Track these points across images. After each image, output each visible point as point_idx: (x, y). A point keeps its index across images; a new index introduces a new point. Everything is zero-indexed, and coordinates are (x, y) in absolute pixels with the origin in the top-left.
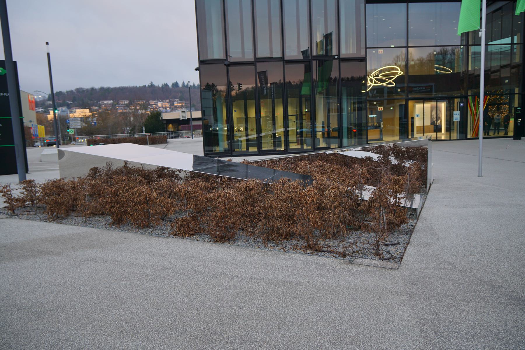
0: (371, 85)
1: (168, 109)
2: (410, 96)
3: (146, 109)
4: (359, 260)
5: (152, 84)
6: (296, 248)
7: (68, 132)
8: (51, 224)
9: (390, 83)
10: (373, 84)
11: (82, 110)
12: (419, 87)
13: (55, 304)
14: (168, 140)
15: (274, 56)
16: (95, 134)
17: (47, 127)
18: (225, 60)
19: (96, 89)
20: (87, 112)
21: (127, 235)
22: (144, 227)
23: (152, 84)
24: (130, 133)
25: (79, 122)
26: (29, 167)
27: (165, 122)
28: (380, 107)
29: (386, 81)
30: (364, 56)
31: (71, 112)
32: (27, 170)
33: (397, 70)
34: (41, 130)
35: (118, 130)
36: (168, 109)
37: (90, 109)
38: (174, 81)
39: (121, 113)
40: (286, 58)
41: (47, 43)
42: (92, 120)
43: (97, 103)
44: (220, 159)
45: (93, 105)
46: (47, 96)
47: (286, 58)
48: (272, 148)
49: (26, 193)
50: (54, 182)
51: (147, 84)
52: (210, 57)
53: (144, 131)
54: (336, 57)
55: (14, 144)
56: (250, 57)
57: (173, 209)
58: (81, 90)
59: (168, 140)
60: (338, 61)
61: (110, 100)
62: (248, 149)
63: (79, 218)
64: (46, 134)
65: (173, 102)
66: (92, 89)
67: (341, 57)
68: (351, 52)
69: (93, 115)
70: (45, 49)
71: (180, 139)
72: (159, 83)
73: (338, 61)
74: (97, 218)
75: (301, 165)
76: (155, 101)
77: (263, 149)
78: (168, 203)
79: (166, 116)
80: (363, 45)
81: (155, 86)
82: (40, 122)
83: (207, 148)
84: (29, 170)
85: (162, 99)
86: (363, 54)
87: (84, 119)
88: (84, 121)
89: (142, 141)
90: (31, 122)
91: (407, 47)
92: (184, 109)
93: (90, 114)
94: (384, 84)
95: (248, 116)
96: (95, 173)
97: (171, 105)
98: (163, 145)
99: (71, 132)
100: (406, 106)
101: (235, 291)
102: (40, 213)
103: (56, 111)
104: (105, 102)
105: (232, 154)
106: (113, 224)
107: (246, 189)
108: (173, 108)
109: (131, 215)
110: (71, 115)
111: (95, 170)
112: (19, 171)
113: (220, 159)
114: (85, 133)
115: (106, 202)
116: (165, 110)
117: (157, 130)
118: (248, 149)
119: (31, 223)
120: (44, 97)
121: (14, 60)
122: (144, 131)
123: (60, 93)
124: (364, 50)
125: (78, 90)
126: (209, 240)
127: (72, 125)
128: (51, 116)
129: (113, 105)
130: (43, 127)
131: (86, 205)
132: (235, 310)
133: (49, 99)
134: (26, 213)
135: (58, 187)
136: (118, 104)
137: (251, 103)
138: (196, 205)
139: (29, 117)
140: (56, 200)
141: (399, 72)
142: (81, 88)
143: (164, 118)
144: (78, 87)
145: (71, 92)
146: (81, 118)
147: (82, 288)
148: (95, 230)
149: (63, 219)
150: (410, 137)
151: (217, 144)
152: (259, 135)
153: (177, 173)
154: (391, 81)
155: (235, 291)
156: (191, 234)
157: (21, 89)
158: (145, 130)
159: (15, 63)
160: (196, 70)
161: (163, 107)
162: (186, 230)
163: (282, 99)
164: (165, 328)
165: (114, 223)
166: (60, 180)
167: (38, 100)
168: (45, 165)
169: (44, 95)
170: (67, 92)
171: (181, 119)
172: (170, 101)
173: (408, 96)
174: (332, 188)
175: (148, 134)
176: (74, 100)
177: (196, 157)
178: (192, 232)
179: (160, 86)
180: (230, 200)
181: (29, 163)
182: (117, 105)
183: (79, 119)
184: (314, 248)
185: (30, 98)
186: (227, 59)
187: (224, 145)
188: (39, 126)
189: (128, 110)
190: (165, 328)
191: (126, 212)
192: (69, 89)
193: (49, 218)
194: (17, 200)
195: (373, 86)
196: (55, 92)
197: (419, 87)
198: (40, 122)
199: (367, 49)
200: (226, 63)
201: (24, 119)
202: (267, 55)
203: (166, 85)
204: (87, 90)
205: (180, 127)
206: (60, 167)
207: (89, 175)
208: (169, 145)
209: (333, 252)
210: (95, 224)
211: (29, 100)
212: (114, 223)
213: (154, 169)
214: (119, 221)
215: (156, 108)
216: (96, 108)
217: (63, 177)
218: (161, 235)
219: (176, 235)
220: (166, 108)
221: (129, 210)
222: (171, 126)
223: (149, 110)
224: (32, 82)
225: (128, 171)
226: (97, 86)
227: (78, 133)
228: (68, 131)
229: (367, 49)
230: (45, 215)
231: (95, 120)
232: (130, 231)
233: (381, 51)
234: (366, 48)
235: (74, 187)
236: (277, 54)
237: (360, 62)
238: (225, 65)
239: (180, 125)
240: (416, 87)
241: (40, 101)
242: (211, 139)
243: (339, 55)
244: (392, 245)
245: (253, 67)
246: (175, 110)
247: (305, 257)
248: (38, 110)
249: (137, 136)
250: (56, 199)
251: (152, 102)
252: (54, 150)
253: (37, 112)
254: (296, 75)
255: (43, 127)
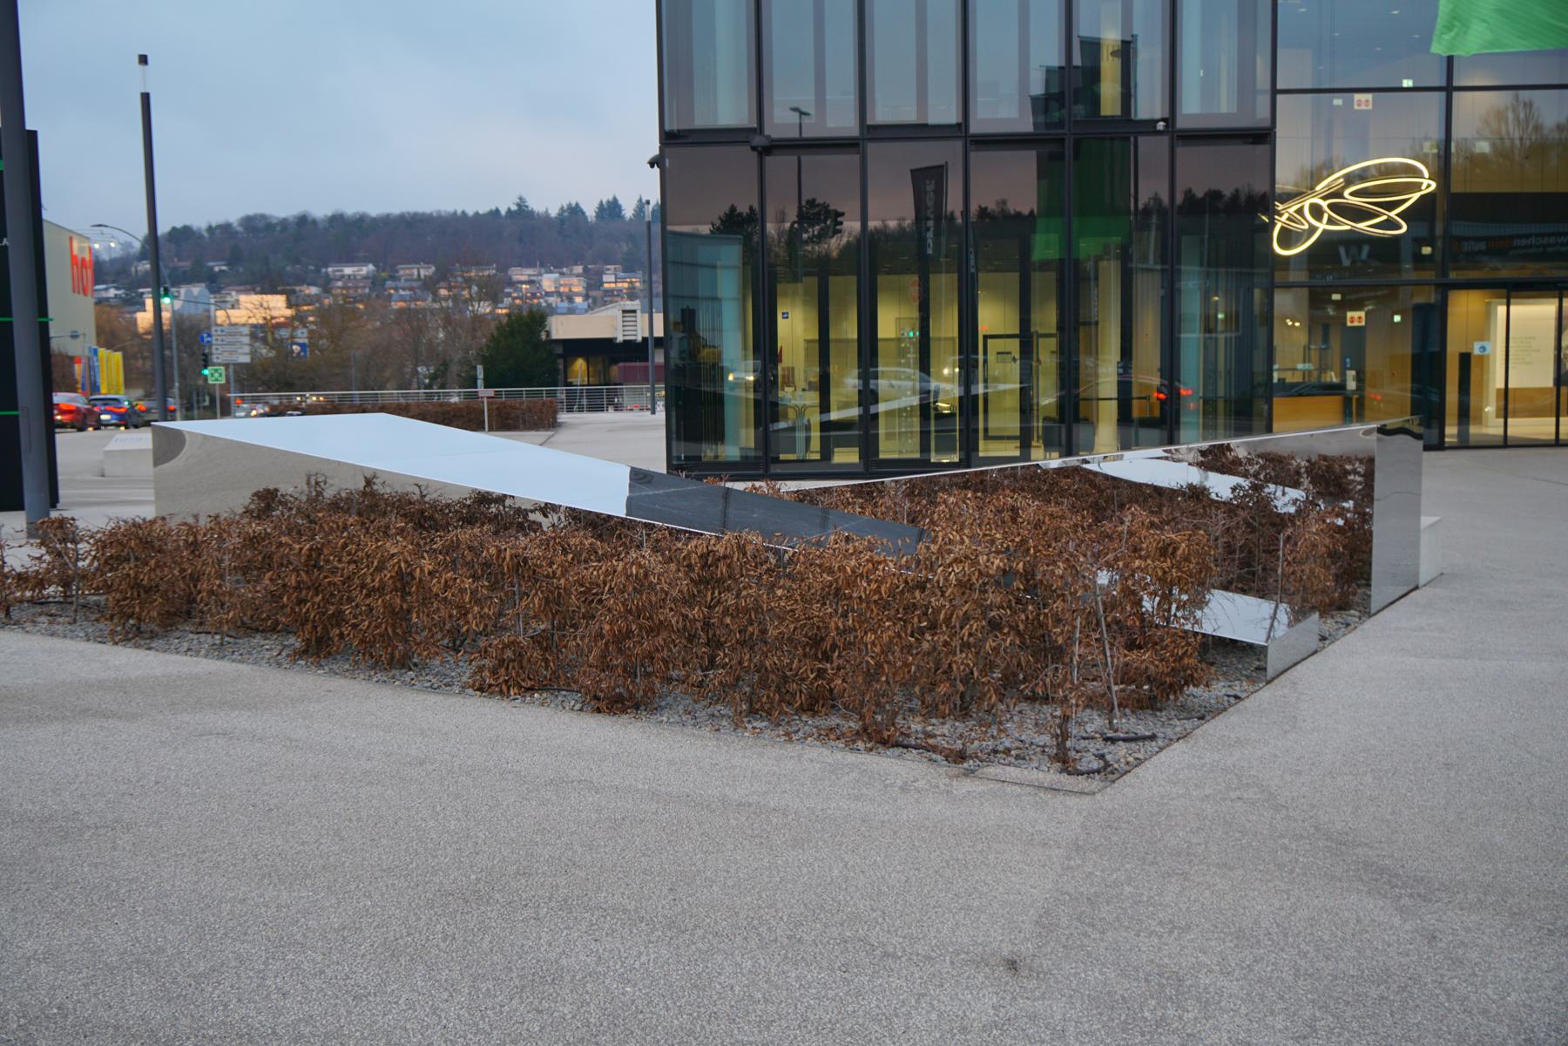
0: (1313, 229)
1: (578, 300)
2: (1453, 275)
3: (495, 299)
4: (991, 770)
5: (521, 204)
6: (828, 735)
7: (206, 378)
8: (119, 648)
9: (1390, 224)
10: (1322, 226)
11: (256, 298)
12: (1543, 235)
13: (110, 816)
14: (563, 417)
15: (932, 120)
16: (280, 379)
17: (135, 357)
18: (752, 130)
19: (314, 222)
20: (277, 305)
21: (338, 683)
22: (391, 664)
23: (521, 204)
24: (429, 387)
25: (246, 340)
26: (62, 492)
27: (559, 350)
28: (1356, 314)
29: (1376, 215)
30: (1267, 124)
31: (221, 305)
32: (54, 500)
33: (1418, 173)
34: (111, 364)
35: (387, 374)
36: (578, 300)
37: (289, 294)
38: (606, 197)
39: (401, 311)
40: (974, 129)
41: (143, 60)
42: (292, 337)
43: (318, 271)
44: (729, 485)
45: (302, 281)
46: (137, 245)
47: (974, 129)
48: (917, 456)
49: (47, 558)
50: (135, 524)
51: (506, 204)
52: (701, 121)
53: (480, 382)
54: (1161, 126)
55: (16, 408)
56: (842, 121)
57: (476, 609)
58: (261, 225)
59: (563, 417)
60: (1166, 139)
61: (365, 261)
62: (826, 454)
63: (203, 637)
64: (128, 383)
65: (600, 274)
66: (303, 220)
67: (1181, 124)
68: (1224, 109)
69: (300, 318)
70: (135, 81)
71: (610, 416)
72: (547, 203)
73: (1166, 139)
74: (258, 639)
75: (945, 502)
76: (530, 271)
77: (882, 456)
78: (462, 591)
79: (563, 328)
80: (1263, 81)
81: (532, 212)
82: (108, 337)
83: (682, 449)
84: (61, 500)
85: (557, 263)
86: (1262, 114)
87: (263, 332)
88: (264, 340)
89: (467, 419)
90: (74, 336)
91: (1449, 89)
92: (629, 305)
93: (289, 312)
94: (1362, 226)
95: (832, 336)
96: (269, 508)
97: (589, 287)
98: (542, 435)
99: (214, 375)
100: (1441, 310)
101: (594, 816)
102: (87, 619)
103: (166, 301)
104: (348, 271)
105: (767, 469)
106: (303, 653)
107: (704, 557)
108: (597, 297)
109: (355, 626)
110: (220, 316)
111: (268, 500)
112: (28, 497)
113: (729, 485)
114: (264, 383)
115: (285, 586)
116: (566, 304)
117: (524, 377)
118: (826, 454)
119: (58, 643)
120: (130, 245)
121: (29, 127)
122: (480, 382)
123: (182, 235)
124: (1267, 99)
125: (249, 222)
126: (578, 706)
127: (219, 354)
128: (144, 319)
129: (375, 282)
130: (118, 356)
131: (223, 594)
132: (575, 852)
133: (142, 256)
134: (43, 619)
135: (146, 544)
136: (393, 278)
137: (844, 287)
138: (547, 601)
139: (72, 317)
140: (136, 578)
141: (1425, 182)
142: (263, 217)
143: (555, 336)
144: (251, 212)
145: (226, 228)
146: (254, 326)
147: (184, 790)
148: (245, 668)
149: (153, 636)
150: (1451, 431)
151: (718, 436)
152: (866, 410)
153: (537, 517)
154: (1393, 214)
155: (594, 816)
156: (528, 689)
157: (45, 215)
158: (485, 379)
159: (33, 135)
160: (652, 164)
161: (559, 294)
162: (517, 675)
163: (854, 278)
164: (378, 874)
165: (305, 652)
166: (153, 522)
167: (105, 257)
168: (109, 476)
169: (124, 238)
170: (210, 229)
171: (620, 339)
172: (586, 270)
173: (1445, 275)
174: (955, 560)
175: (491, 392)
176: (234, 259)
177: (639, 477)
178: (529, 683)
179: (554, 213)
180: (642, 583)
181: (60, 478)
182: (389, 283)
183: (246, 330)
184: (881, 738)
185: (76, 252)
186: (760, 129)
187: (740, 440)
188: (102, 352)
189: (428, 303)
190: (378, 874)
191: (338, 619)
192: (217, 219)
193: (113, 633)
194: (22, 578)
195: (1325, 231)
196: (163, 228)
197: (1543, 235)
198: (108, 337)
199: (1279, 97)
200: (758, 141)
201: (51, 324)
202: (908, 115)
203: (575, 211)
204: (284, 223)
205: (615, 370)
206: (157, 493)
207: (247, 511)
208: (561, 436)
209: (934, 749)
210: (249, 653)
211: (74, 258)
212: (305, 652)
213: (456, 498)
214: (319, 648)
215: (534, 296)
216: (314, 290)
217: (164, 514)
218: (443, 685)
219: (481, 689)
220: (570, 299)
221: (347, 609)
222: (580, 364)
223: (507, 301)
224: (88, 198)
225: (373, 503)
226: (321, 210)
227: (239, 381)
228: (206, 372)
229: (1279, 97)
230: (101, 626)
231: (302, 335)
232: (351, 674)
233: (1363, 101)
234: (1275, 92)
235: (195, 542)
236: (944, 112)
237: (1250, 147)
238: (754, 149)
239: (614, 361)
240: (1527, 236)
241: (113, 261)
242: (694, 413)
243: (1170, 120)
244: (1124, 740)
245: (856, 158)
246: (605, 303)
247: (851, 758)
248: (104, 295)
249: (455, 399)
250: (137, 573)
251: (520, 274)
252: (142, 440)
253: (100, 302)
254: (1013, 185)
255: (118, 356)
